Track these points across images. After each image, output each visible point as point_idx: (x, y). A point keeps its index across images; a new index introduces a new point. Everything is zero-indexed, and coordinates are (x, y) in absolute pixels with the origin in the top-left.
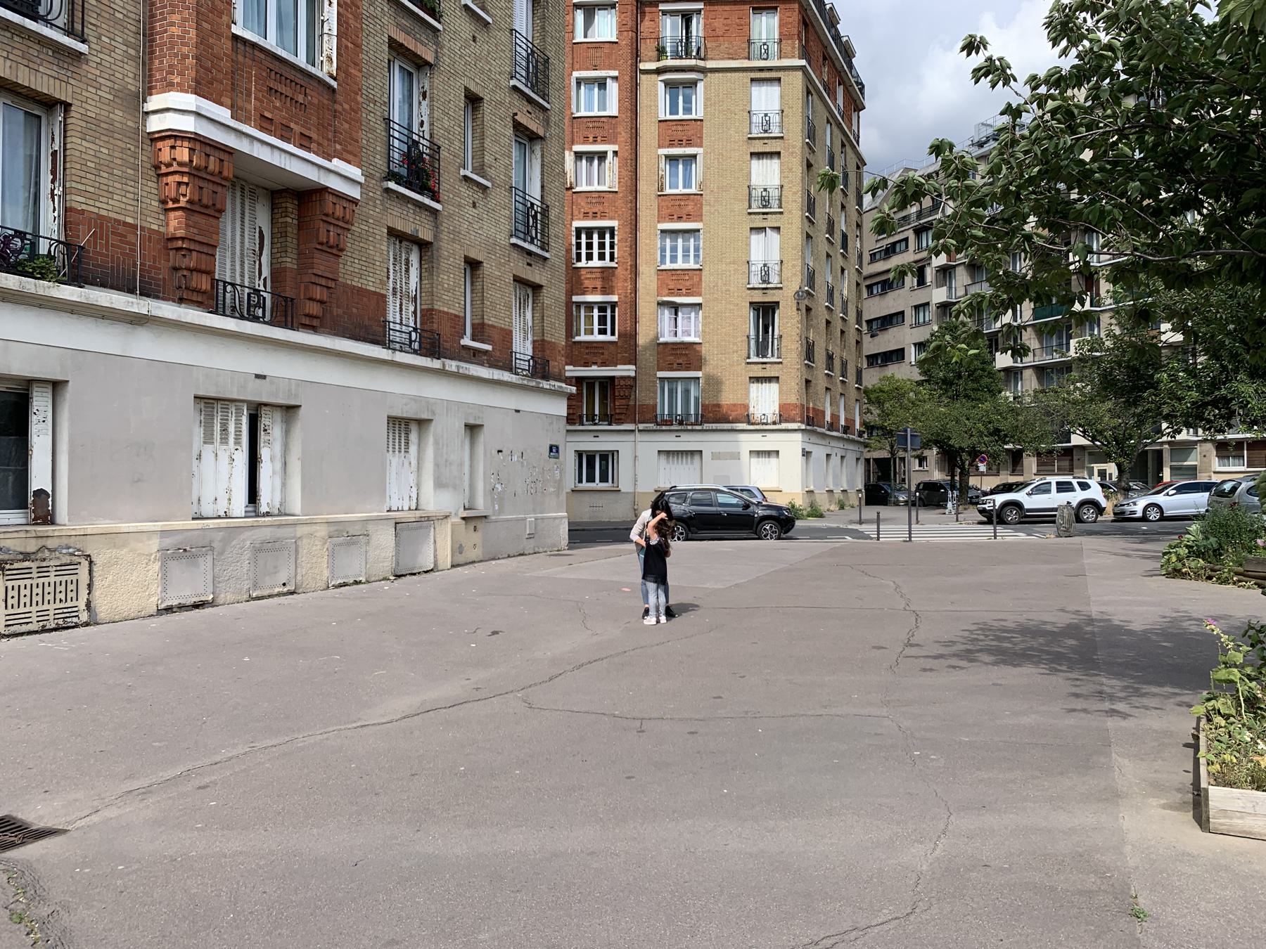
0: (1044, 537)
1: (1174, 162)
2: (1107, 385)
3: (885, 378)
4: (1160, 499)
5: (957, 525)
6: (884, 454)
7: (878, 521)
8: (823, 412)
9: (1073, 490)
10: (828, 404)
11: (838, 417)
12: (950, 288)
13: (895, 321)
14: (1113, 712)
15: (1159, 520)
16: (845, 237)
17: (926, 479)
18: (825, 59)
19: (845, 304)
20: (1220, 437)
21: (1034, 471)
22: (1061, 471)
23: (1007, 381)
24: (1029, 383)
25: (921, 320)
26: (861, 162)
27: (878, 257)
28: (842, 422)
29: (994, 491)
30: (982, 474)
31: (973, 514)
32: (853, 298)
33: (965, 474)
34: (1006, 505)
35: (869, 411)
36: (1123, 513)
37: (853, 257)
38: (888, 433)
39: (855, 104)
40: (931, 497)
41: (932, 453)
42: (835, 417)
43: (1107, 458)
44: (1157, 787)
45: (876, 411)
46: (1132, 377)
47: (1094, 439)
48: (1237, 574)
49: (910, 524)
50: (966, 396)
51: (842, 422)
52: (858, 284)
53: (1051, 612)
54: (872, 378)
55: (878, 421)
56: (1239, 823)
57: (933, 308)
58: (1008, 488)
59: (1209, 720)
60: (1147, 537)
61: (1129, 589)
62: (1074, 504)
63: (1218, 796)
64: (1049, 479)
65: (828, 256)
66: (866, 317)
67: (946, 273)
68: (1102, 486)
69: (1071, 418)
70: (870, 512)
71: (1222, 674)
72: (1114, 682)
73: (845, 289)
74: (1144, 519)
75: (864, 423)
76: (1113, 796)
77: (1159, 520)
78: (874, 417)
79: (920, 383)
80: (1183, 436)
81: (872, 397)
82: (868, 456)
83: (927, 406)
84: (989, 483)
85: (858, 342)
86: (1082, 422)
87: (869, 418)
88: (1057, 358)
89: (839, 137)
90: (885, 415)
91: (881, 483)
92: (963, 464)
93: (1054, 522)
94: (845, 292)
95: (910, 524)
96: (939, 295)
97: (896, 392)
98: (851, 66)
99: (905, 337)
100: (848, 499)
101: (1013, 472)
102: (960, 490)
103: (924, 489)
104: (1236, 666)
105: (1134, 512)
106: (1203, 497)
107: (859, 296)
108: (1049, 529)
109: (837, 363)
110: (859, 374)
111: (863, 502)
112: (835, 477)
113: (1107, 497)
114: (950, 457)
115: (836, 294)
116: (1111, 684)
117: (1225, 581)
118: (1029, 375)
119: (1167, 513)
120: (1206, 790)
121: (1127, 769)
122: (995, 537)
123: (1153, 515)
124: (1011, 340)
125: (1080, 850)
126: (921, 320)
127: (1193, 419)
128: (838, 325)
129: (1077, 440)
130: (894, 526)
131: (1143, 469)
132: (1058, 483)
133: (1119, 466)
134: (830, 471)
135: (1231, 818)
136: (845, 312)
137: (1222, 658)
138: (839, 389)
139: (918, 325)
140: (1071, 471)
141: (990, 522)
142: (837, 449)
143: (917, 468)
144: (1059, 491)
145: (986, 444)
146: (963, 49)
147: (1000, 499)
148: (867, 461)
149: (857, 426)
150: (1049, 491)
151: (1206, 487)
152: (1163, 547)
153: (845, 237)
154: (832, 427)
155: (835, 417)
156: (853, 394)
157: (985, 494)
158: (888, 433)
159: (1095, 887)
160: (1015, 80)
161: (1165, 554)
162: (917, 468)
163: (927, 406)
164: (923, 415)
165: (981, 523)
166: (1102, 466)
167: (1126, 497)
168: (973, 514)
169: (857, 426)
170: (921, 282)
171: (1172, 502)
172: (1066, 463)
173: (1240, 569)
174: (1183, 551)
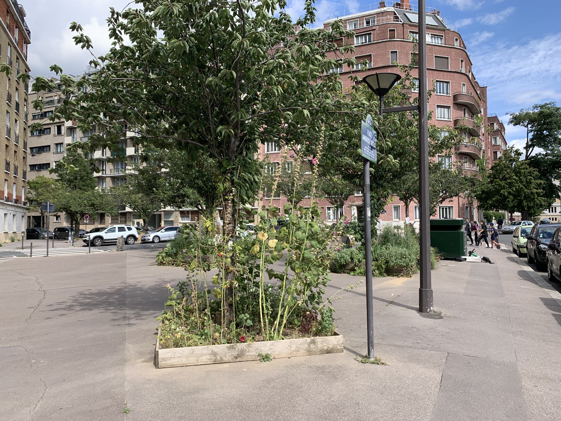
0: (112, 251)
1: (157, 99)
2: (140, 188)
3: (39, 177)
4: (159, 234)
5: (73, 248)
6: (38, 214)
7: (31, 247)
8: (3, 192)
9: (125, 230)
10: (6, 188)
11: (12, 195)
12: (73, 137)
13: (45, 149)
14: (130, 325)
15: (159, 242)
16: (17, 105)
17: (59, 226)
18: (8, 12)
19: (17, 138)
20: (180, 209)
21: (110, 222)
22: (121, 223)
23: (99, 182)
24: (108, 184)
25: (59, 151)
26: (28, 69)
27: (37, 117)
28: (14, 197)
29: (91, 232)
30: (86, 224)
31: (81, 242)
32: (22, 135)
33: (78, 224)
34: (95, 238)
35: (30, 192)
36: (145, 240)
37: (22, 115)
38: (39, 204)
39: (25, 39)
40: (61, 234)
41: (63, 214)
42: (10, 195)
43: (140, 217)
44: (141, 354)
45: (34, 193)
46: (148, 184)
47: (134, 209)
48: (182, 262)
49: (48, 248)
50: (80, 189)
51: (14, 197)
52: (25, 129)
53: (108, 284)
54: (32, 176)
55: (35, 198)
56: (169, 362)
57: (65, 145)
58: (97, 230)
59: (163, 322)
60: (153, 249)
61: (143, 271)
62: (125, 237)
63: (163, 353)
64: (115, 226)
65: (8, 112)
66: (29, 145)
67: (71, 130)
68: (137, 229)
69: (125, 200)
70: (28, 243)
71: (169, 303)
72: (131, 312)
73: (18, 130)
74: (153, 242)
75: (27, 198)
76: (123, 362)
77: (159, 242)
78: (33, 195)
79: (57, 181)
80: (168, 208)
81: (33, 186)
82: (30, 214)
83: (60, 192)
84: (89, 228)
85: (24, 158)
86: (130, 201)
87: (30, 196)
88: (121, 174)
89: (15, 54)
90: (38, 194)
91: (35, 228)
92: (77, 219)
93: (116, 245)
94: (17, 132)
95: (48, 248)
96: (68, 140)
97: (46, 184)
98: (23, 21)
99: (51, 158)
100: (17, 236)
101: (101, 223)
102: (75, 231)
103: (58, 231)
104: (174, 300)
105: (149, 239)
106: (174, 232)
107: (25, 135)
108: (114, 248)
109: (12, 167)
110: (24, 176)
111: (25, 238)
112: (9, 225)
113: (139, 233)
114: (72, 216)
115: (12, 132)
116: (129, 312)
117: (178, 266)
118: (108, 180)
119: (162, 239)
120: (158, 351)
121: (131, 349)
122: (90, 252)
123: (156, 240)
124: (95, 165)
125: (106, 389)
126: (59, 151)
127: (172, 201)
128: (13, 148)
129: (128, 209)
130: (40, 248)
131: (154, 222)
132: (119, 228)
133: (144, 220)
134: (7, 223)
135: (166, 361)
136: (17, 141)
137: (170, 298)
138: (13, 180)
139: (57, 153)
140: (125, 222)
141: (88, 246)
142: (11, 211)
143: (55, 221)
144: (119, 231)
145: (89, 210)
146: (70, 28)
147: (93, 235)
148: (29, 217)
149: (23, 200)
150: (114, 231)
151: (175, 229)
152: (156, 253)
153: (17, 105)
154: (8, 199)
155: (10, 195)
156: (21, 184)
157: (87, 233)
158: (39, 204)
159: (110, 405)
160: (92, 47)
161: (157, 256)
162: (55, 221)
163: (60, 192)
164: (58, 196)
165: (84, 246)
166: (138, 220)
167: (147, 233)
168: (81, 242)
169: (23, 200)
170: (59, 132)
171: (164, 235)
172: (124, 219)
173: (184, 260)
174: (164, 254)
